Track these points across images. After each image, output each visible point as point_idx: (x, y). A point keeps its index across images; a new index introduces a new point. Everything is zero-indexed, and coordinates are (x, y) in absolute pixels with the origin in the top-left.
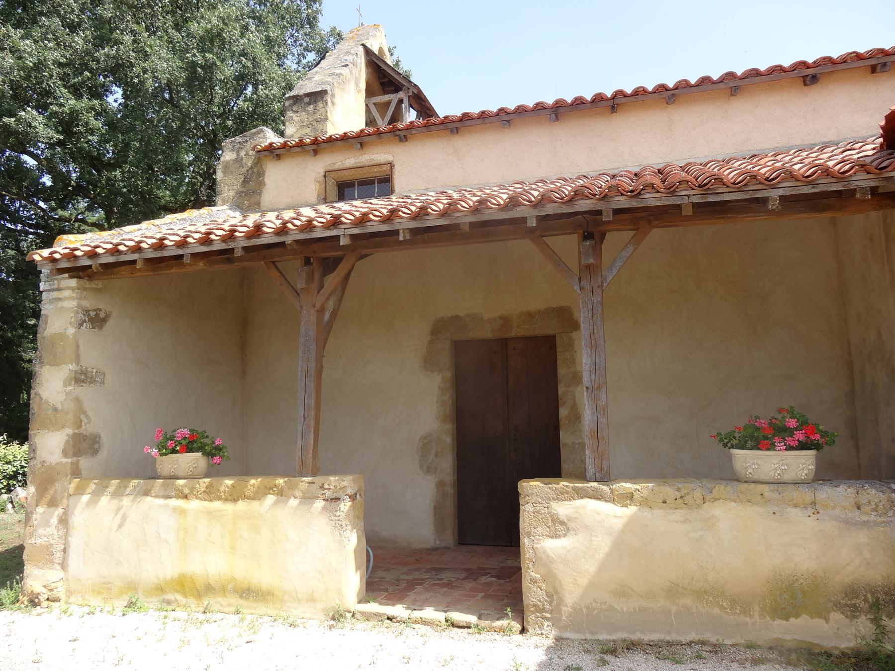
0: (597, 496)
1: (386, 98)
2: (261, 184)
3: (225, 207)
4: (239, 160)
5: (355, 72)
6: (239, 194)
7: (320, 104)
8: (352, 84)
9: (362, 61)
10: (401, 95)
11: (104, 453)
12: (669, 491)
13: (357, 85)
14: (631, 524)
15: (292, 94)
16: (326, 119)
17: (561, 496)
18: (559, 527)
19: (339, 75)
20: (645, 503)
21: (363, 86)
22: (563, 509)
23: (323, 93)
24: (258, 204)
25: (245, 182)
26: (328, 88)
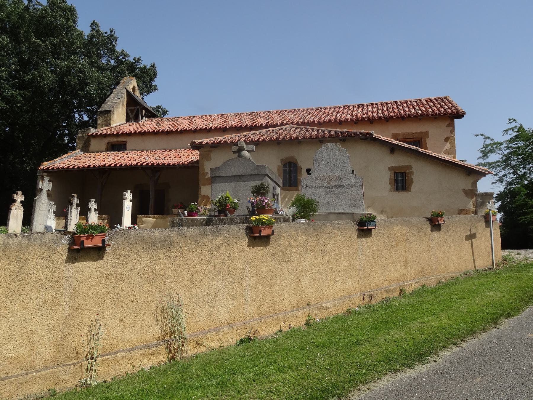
0: (150, 217)
1: (133, 108)
2: (90, 144)
3: (78, 150)
4: (83, 137)
5: (122, 100)
6: (83, 147)
7: (109, 115)
8: (121, 105)
9: (125, 95)
10: (138, 107)
11: (258, 183)
12: (161, 216)
13: (123, 104)
14: (155, 221)
15: (100, 110)
16: (111, 119)
17: (144, 217)
18: (143, 223)
19: (116, 103)
20: (157, 218)
21: (125, 103)
22: (144, 220)
23: (110, 111)
24: (88, 150)
25: (84, 143)
26: (112, 109)
